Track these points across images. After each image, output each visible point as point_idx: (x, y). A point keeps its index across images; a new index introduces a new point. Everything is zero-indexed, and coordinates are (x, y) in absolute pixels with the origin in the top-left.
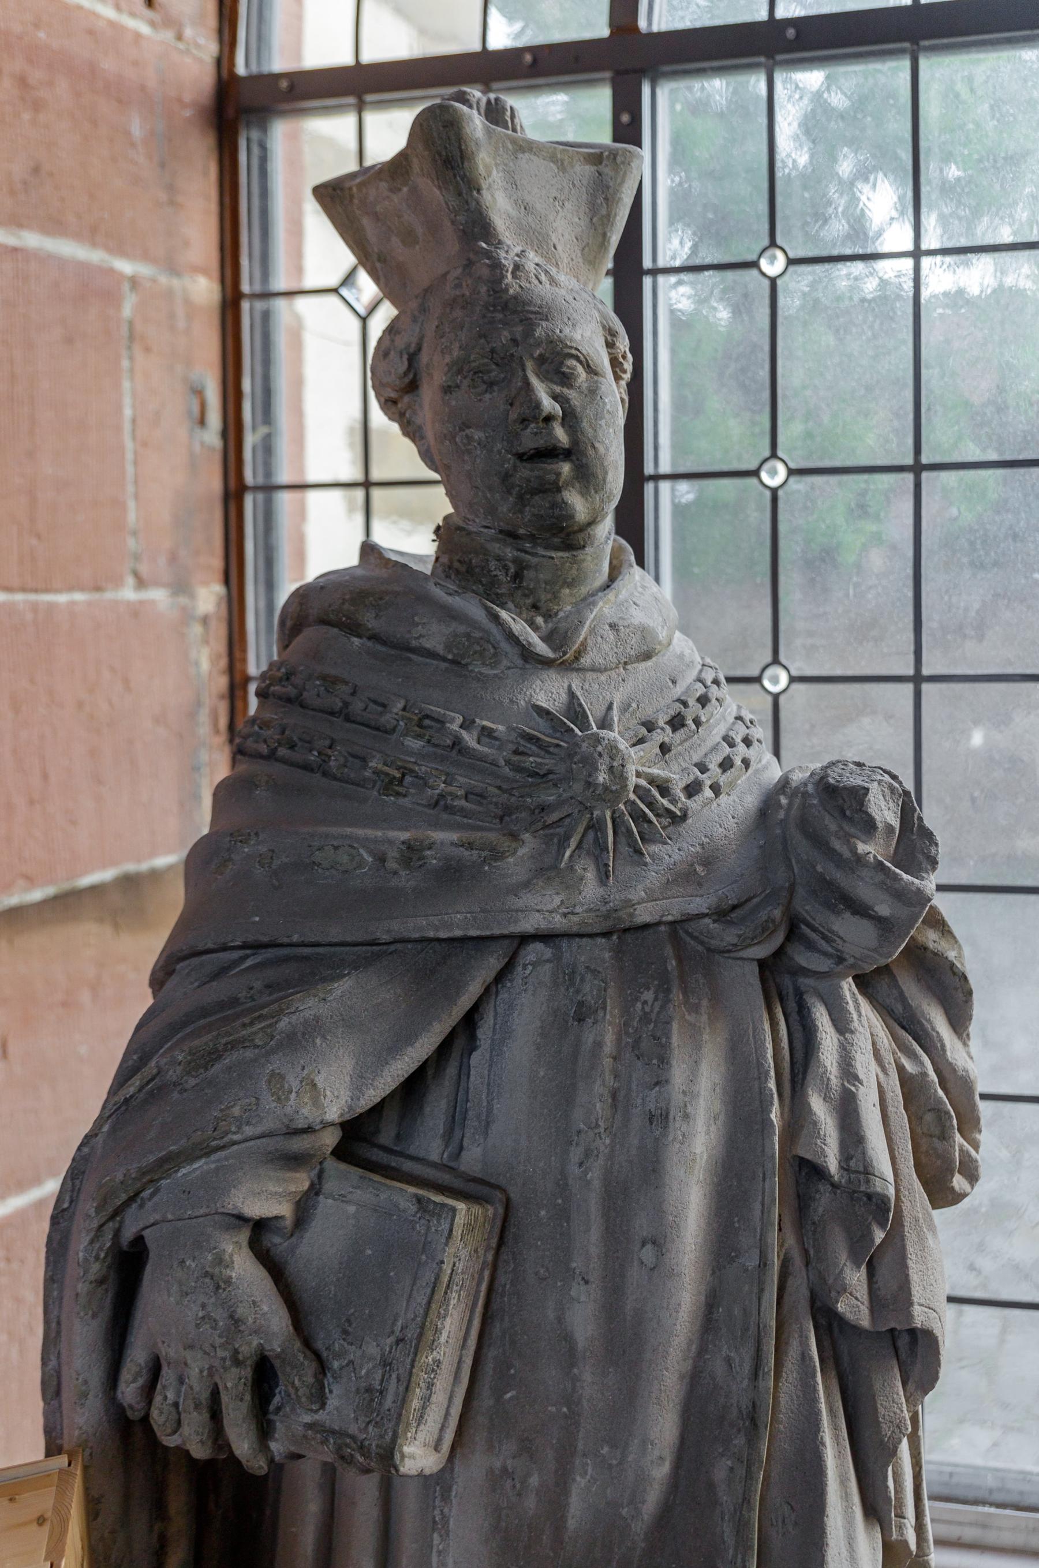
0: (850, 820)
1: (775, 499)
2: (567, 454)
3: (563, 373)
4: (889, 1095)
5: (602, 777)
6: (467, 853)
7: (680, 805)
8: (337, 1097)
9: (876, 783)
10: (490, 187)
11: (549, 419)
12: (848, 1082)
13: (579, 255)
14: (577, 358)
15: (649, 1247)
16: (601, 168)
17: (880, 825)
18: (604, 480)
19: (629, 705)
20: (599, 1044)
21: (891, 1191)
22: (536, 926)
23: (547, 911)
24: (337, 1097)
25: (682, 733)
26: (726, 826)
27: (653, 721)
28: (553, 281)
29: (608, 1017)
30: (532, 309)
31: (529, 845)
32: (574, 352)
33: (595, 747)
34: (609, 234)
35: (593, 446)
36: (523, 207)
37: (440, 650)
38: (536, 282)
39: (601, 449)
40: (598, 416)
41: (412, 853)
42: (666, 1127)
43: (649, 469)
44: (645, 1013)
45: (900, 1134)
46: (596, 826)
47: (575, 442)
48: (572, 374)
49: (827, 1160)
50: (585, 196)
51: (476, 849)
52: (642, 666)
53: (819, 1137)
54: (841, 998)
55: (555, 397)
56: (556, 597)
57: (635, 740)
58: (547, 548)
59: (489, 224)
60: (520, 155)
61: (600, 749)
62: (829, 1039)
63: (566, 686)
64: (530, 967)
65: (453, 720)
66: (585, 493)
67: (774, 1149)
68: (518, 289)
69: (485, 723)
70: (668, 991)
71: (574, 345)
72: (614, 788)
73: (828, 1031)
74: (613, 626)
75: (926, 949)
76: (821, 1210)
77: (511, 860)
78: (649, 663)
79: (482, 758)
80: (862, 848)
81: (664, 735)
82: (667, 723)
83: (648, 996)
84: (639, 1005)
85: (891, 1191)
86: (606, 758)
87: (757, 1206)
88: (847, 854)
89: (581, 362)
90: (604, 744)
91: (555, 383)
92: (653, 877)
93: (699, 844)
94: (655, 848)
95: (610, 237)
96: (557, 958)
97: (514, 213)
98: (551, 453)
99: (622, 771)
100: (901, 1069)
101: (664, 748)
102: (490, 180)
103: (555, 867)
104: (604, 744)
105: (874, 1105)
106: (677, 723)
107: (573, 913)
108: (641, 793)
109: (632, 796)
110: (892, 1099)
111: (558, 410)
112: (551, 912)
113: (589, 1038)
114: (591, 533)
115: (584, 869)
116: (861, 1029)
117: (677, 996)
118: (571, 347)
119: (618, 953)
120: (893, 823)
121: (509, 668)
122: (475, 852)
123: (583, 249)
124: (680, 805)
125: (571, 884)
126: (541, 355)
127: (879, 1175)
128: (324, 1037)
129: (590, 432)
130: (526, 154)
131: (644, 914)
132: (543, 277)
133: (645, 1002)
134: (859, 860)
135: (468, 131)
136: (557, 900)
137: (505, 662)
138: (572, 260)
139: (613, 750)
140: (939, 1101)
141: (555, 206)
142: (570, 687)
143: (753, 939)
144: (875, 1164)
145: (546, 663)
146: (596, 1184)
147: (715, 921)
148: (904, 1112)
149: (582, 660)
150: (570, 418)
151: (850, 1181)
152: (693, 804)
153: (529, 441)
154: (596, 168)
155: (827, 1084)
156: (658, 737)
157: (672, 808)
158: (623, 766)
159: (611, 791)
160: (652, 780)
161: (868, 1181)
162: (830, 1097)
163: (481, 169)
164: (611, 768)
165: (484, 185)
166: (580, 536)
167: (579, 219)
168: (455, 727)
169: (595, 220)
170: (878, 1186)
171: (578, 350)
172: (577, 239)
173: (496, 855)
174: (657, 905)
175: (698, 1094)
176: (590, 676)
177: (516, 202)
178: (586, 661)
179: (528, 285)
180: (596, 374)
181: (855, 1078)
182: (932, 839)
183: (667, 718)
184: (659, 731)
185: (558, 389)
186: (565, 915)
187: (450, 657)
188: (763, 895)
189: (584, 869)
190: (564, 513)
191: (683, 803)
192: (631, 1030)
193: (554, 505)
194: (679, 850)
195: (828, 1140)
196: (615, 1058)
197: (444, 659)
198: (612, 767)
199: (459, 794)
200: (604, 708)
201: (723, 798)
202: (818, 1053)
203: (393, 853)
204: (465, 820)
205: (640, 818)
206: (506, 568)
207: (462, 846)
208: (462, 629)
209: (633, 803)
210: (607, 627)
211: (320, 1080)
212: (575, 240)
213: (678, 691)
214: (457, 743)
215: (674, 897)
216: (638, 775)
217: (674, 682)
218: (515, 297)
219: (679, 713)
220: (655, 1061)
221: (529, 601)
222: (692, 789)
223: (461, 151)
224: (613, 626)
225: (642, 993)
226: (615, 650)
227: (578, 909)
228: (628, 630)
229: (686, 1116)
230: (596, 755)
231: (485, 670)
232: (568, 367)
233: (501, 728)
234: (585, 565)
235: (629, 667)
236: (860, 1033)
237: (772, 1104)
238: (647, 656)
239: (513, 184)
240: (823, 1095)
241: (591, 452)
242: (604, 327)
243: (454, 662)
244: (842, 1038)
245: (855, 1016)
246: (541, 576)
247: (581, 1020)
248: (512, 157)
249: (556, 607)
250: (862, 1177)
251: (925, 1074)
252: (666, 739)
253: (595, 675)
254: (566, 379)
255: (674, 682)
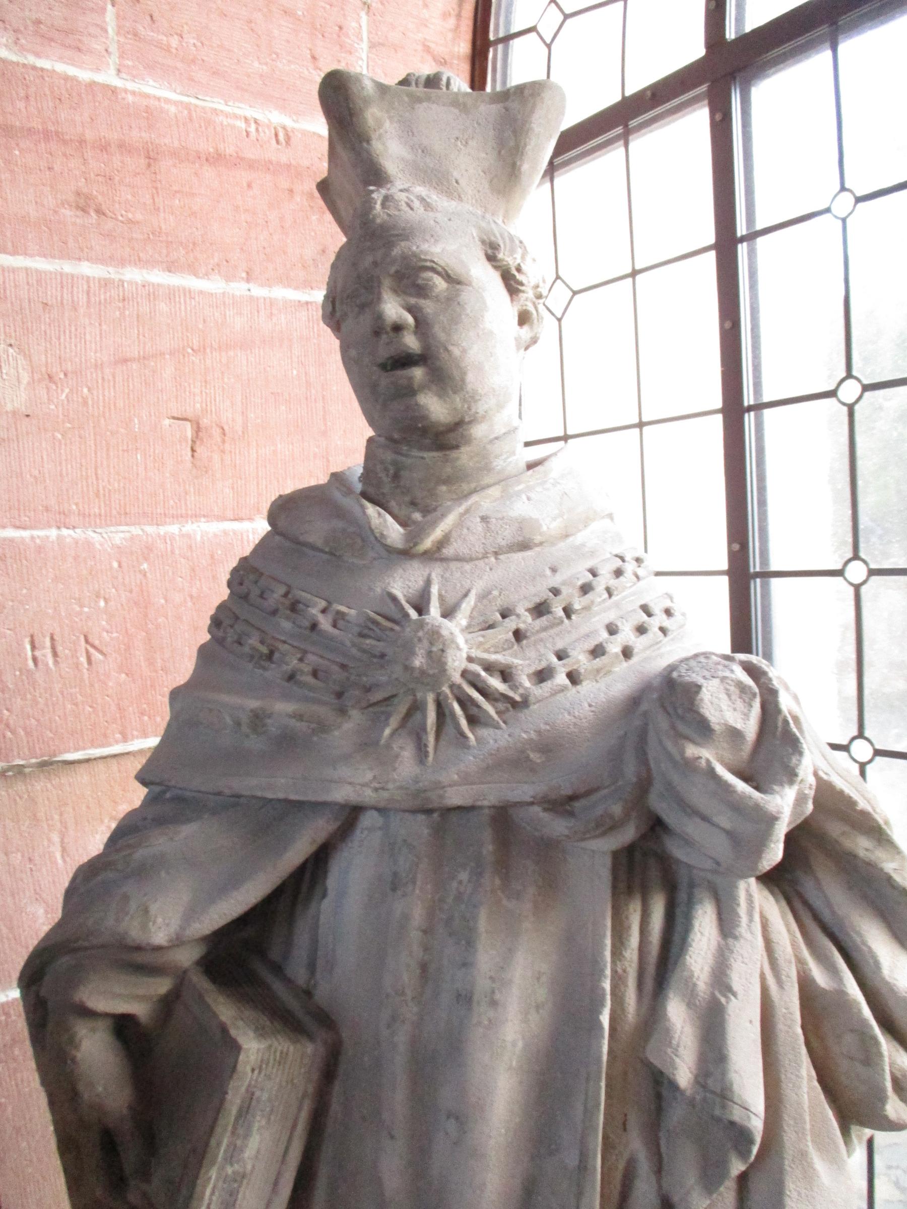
0: (682, 718)
1: (851, 414)
2: (421, 359)
3: (418, 286)
4: (780, 1011)
5: (418, 661)
6: (298, 724)
7: (521, 691)
8: (168, 925)
9: (716, 682)
10: (380, 137)
11: (398, 328)
12: (720, 992)
13: (487, 186)
14: (433, 270)
15: (453, 1121)
16: (509, 104)
17: (716, 727)
18: (463, 380)
19: (490, 593)
20: (406, 917)
21: (757, 1125)
22: (346, 798)
23: (359, 784)
24: (168, 925)
25: (544, 620)
26: (577, 714)
27: (511, 608)
28: (427, 206)
29: (417, 891)
30: (396, 232)
31: (356, 718)
32: (428, 264)
33: (417, 631)
34: (518, 163)
35: (446, 350)
36: (420, 151)
37: (319, 543)
38: (407, 209)
39: (456, 352)
40: (455, 320)
41: (258, 719)
42: (470, 1009)
43: (749, 399)
44: (460, 893)
45: (791, 1057)
46: (416, 707)
47: (427, 347)
48: (427, 284)
49: (675, 1072)
50: (492, 133)
51: (307, 721)
52: (520, 555)
53: (671, 1047)
54: (734, 899)
55: (410, 309)
56: (432, 494)
57: (484, 625)
58: (421, 449)
59: (381, 170)
60: (417, 106)
61: (420, 634)
62: (705, 940)
63: (426, 574)
64: (366, 832)
65: (314, 605)
66: (442, 394)
67: (601, 1052)
68: (385, 217)
69: (343, 609)
70: (480, 875)
71: (428, 257)
72: (431, 672)
73: (706, 934)
74: (484, 519)
75: (855, 856)
76: (675, 1119)
77: (336, 733)
78: (528, 553)
79: (332, 638)
80: (691, 751)
81: (526, 621)
82: (528, 610)
83: (464, 876)
84: (455, 884)
85: (757, 1125)
86: (426, 643)
87: (580, 1107)
88: (678, 757)
89: (438, 273)
90: (426, 630)
91: (411, 295)
92: (470, 761)
93: (535, 731)
94: (484, 732)
95: (521, 166)
96: (385, 828)
97: (409, 156)
98: (405, 361)
99: (441, 656)
100: (806, 987)
101: (518, 635)
102: (381, 131)
103: (376, 743)
104: (426, 630)
105: (751, 1022)
106: (540, 610)
107: (383, 789)
108: (470, 677)
109: (457, 678)
110: (783, 1016)
111: (410, 320)
112: (363, 785)
113: (398, 908)
114: (465, 433)
115: (401, 748)
116: (748, 936)
117: (491, 881)
118: (426, 260)
119: (439, 832)
120: (739, 726)
121: (375, 559)
122: (303, 723)
123: (491, 181)
124: (521, 691)
125: (387, 760)
126: (397, 272)
127: (740, 1103)
128: (168, 873)
129: (442, 336)
130: (424, 104)
131: (455, 797)
132: (416, 204)
133: (460, 882)
134: (689, 766)
135: (355, 91)
136: (369, 776)
137: (371, 554)
138: (479, 191)
139: (435, 635)
140: (864, 1022)
141: (457, 146)
142: (429, 575)
143: (584, 833)
144: (736, 1087)
145: (406, 554)
146: (402, 1048)
147: (545, 810)
148: (799, 1031)
149: (444, 551)
150: (422, 325)
151: (704, 1099)
152: (538, 691)
153: (384, 352)
154: (502, 105)
155: (692, 991)
156: (511, 624)
157: (511, 694)
158: (443, 651)
159: (429, 675)
160: (489, 668)
161: (724, 1107)
162: (695, 1005)
163: (371, 122)
164: (429, 653)
165: (374, 136)
166: (451, 435)
167: (487, 154)
168: (314, 611)
169: (503, 152)
170: (737, 1115)
171: (434, 262)
172: (485, 173)
173: (322, 728)
174: (472, 789)
175: (511, 981)
176: (453, 565)
177: (412, 148)
178: (448, 551)
179: (397, 213)
180: (459, 282)
181: (728, 990)
182: (797, 747)
183: (530, 605)
184: (513, 617)
185: (413, 301)
186: (376, 790)
187: (327, 550)
188: (613, 787)
189: (401, 748)
190: (417, 414)
191: (526, 689)
192: (446, 907)
193: (408, 408)
194: (509, 735)
195: (681, 1050)
196: (425, 932)
197: (321, 551)
198: (431, 652)
199: (306, 670)
200: (460, 594)
201: (587, 687)
202: (685, 955)
203: (245, 719)
204: (312, 694)
205: (465, 702)
206: (386, 470)
207: (294, 717)
208: (339, 524)
209: (459, 687)
210: (478, 520)
211: (154, 908)
212: (482, 174)
213: (555, 581)
214: (314, 626)
215: (495, 783)
216: (470, 659)
217: (554, 570)
218: (381, 226)
219: (545, 601)
220: (463, 942)
221: (407, 499)
222: (542, 676)
223: (349, 109)
224: (484, 519)
225: (459, 872)
226: (484, 541)
227: (390, 786)
228: (501, 522)
229: (494, 1003)
230: (416, 640)
231: (355, 561)
232: (424, 279)
233: (353, 612)
234: (459, 463)
235: (501, 557)
236: (746, 939)
237: (603, 1005)
238: (524, 546)
239: (408, 130)
240: (687, 1000)
241: (444, 355)
242: (483, 242)
243: (331, 554)
244: (723, 942)
245: (744, 919)
246: (415, 475)
247: (394, 889)
248: (409, 108)
249: (434, 503)
250: (718, 1100)
251: (841, 993)
252: (522, 626)
253: (459, 564)
254: (422, 291)
255: (554, 570)
